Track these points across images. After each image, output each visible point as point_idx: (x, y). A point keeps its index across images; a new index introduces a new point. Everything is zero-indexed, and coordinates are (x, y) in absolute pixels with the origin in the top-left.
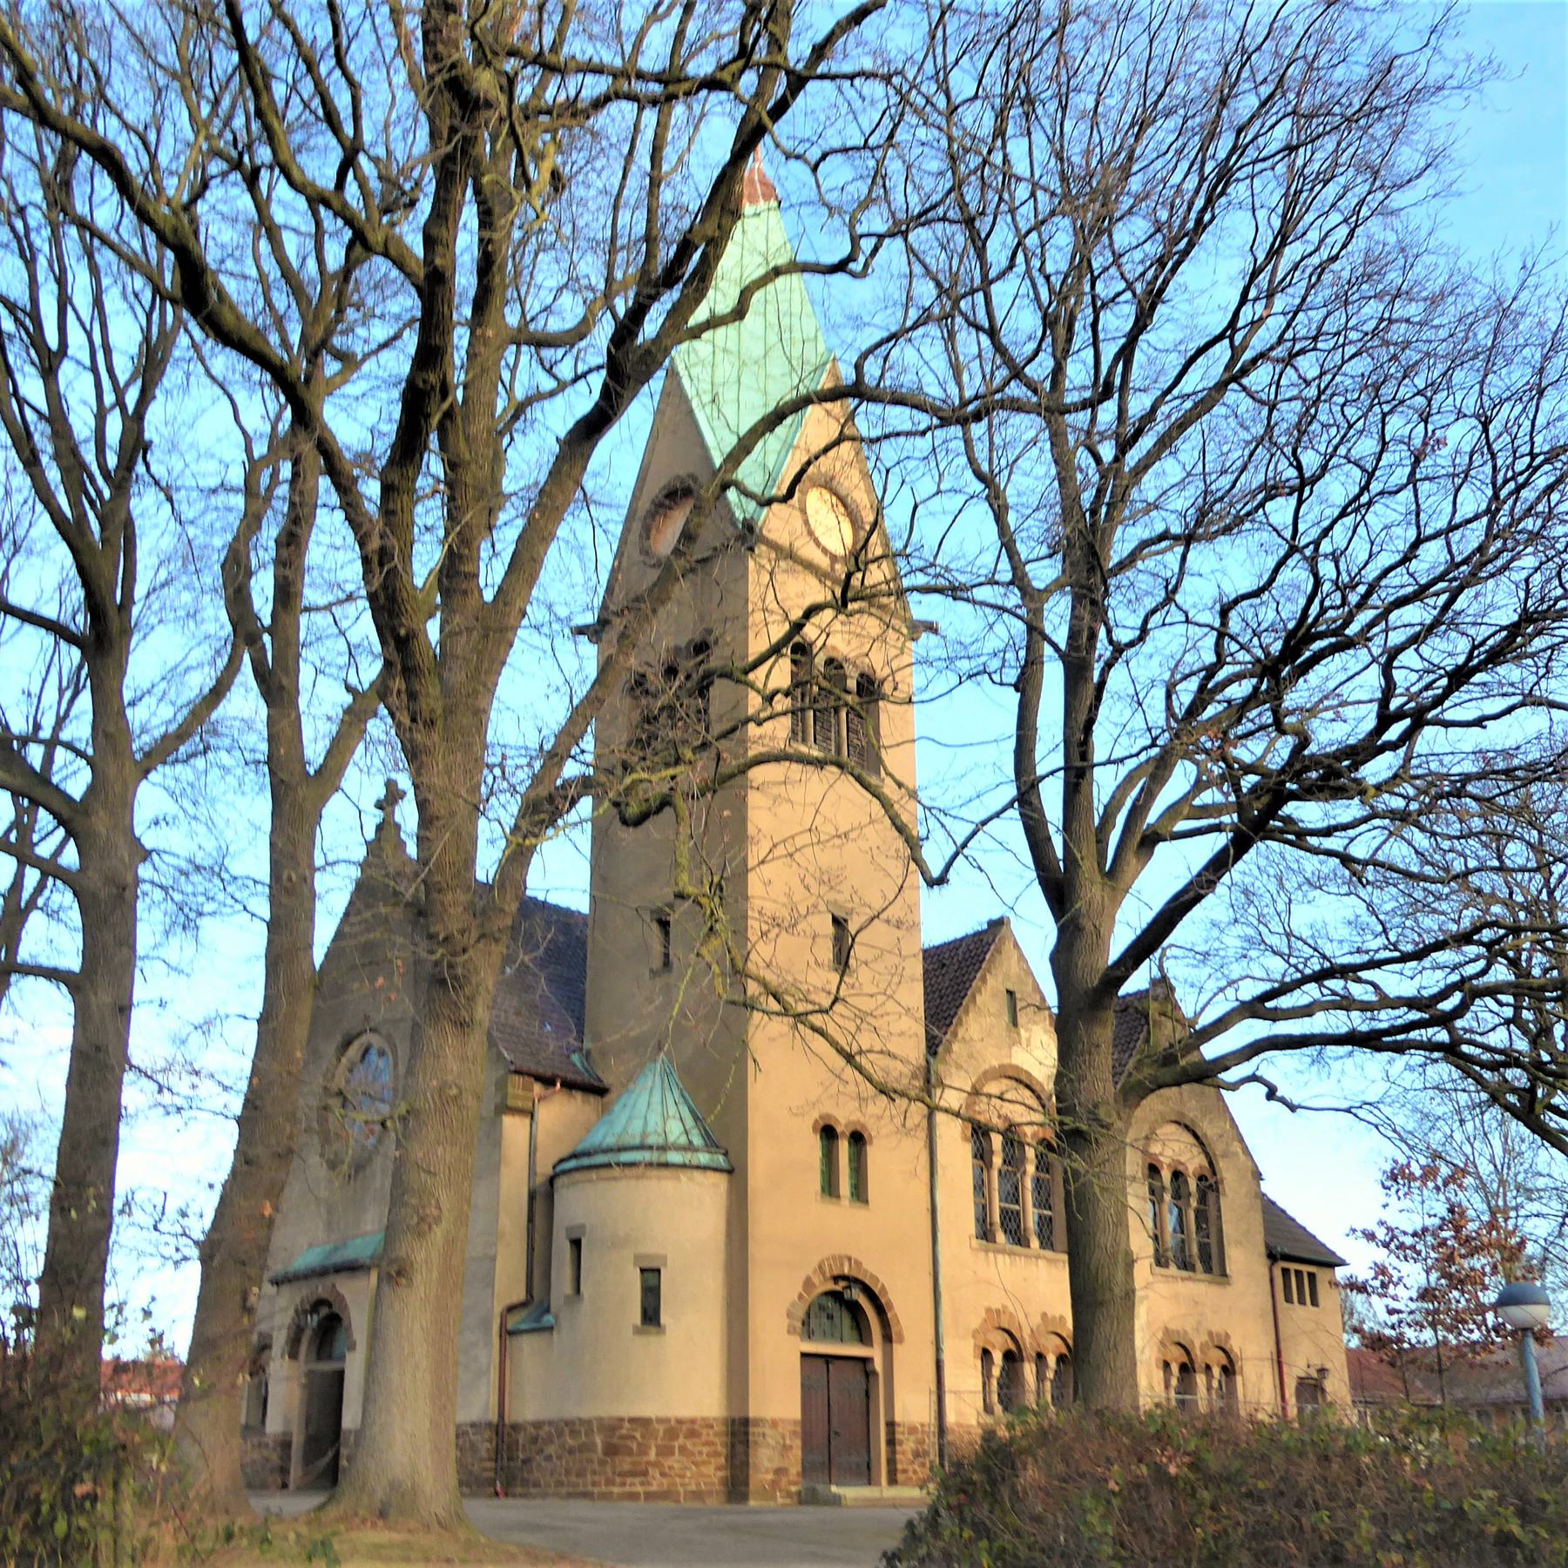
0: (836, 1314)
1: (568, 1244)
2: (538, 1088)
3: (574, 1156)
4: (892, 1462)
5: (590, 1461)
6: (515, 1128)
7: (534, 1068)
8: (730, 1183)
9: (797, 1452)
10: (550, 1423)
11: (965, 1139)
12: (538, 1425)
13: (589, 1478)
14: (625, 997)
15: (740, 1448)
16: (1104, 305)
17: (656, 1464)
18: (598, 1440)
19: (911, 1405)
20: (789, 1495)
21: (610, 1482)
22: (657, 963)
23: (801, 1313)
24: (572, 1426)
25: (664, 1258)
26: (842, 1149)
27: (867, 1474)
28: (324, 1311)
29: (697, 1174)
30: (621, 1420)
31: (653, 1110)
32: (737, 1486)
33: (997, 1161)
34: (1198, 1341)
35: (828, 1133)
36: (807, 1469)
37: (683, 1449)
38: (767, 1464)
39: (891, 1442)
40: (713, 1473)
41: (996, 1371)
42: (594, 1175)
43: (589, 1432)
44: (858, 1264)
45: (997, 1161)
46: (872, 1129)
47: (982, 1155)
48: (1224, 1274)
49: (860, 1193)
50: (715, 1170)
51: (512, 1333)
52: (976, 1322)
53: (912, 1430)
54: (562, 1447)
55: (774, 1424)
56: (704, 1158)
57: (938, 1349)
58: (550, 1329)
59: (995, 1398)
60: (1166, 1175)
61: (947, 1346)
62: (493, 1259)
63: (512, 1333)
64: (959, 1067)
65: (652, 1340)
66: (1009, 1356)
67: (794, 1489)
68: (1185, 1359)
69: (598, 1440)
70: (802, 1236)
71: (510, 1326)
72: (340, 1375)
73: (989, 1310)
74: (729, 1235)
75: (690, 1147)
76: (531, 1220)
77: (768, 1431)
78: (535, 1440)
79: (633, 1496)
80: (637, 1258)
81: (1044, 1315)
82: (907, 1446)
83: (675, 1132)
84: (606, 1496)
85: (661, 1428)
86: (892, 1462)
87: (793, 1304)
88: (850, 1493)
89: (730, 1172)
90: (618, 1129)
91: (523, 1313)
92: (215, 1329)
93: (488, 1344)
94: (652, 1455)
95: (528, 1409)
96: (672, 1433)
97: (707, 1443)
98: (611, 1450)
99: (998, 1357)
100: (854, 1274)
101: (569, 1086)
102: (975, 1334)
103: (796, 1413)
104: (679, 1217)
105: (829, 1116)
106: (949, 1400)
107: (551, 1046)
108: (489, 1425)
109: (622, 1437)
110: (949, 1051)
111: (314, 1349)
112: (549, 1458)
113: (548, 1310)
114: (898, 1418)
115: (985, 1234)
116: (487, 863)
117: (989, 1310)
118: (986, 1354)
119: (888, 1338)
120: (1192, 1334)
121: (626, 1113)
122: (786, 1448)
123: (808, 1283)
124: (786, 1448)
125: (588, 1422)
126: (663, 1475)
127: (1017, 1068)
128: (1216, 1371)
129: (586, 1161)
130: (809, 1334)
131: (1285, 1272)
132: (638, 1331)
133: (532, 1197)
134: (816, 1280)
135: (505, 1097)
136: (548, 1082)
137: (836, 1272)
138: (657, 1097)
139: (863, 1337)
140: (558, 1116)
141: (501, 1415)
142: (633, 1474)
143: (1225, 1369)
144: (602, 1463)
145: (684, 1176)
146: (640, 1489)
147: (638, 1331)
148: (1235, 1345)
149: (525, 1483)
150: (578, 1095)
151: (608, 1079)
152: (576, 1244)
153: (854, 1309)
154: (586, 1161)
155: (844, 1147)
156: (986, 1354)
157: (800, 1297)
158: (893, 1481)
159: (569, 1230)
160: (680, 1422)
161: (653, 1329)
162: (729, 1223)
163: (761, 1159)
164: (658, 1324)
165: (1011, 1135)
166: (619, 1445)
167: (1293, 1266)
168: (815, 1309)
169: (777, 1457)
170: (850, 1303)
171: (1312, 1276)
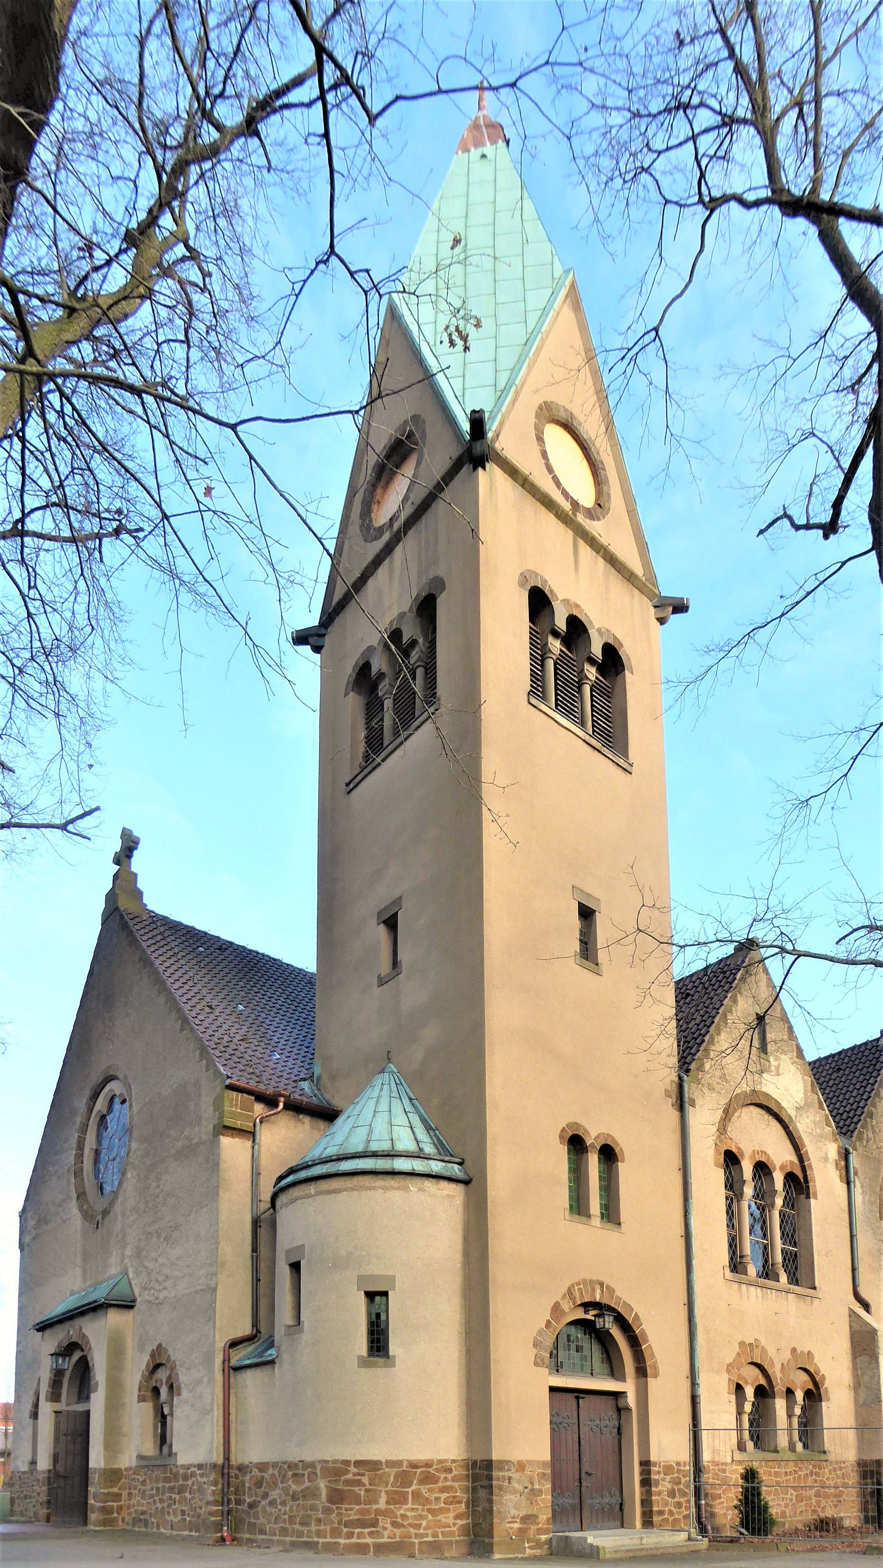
0: (586, 1344)
1: (287, 1270)
2: (259, 1109)
3: (292, 1171)
4: (646, 1503)
5: (313, 1508)
6: (233, 1149)
7: (253, 1085)
8: (467, 1195)
9: (547, 1497)
10: (275, 1465)
11: (717, 1165)
12: (262, 1467)
13: (313, 1528)
14: (354, 1018)
15: (482, 1493)
16: (578, 1398)
17: (386, 1513)
18: (322, 1485)
19: (668, 1444)
20: (539, 1544)
21: (336, 1533)
22: (385, 967)
23: (549, 1342)
24: (295, 1469)
25: (392, 1279)
26: (592, 1159)
27: (618, 1516)
28: (76, 1356)
29: (428, 1184)
30: (347, 1463)
31: (380, 1118)
32: (479, 1538)
33: (749, 1191)
35: (576, 1143)
36: (558, 1513)
37: (416, 1495)
38: (513, 1512)
39: (646, 1482)
40: (452, 1521)
41: (748, 1407)
42: (312, 1188)
43: (313, 1476)
44: (611, 1290)
45: (749, 1191)
46: (624, 1144)
47: (733, 1185)
49: (611, 1213)
50: (450, 1179)
51: (236, 1369)
53: (668, 1470)
54: (286, 1490)
55: (521, 1466)
56: (436, 1167)
57: (694, 1384)
58: (272, 1362)
59: (746, 1434)
61: (703, 1379)
62: (215, 1290)
63: (236, 1369)
64: (711, 1088)
65: (378, 1373)
67: (544, 1537)
68: (811, 1386)
69: (322, 1485)
70: (548, 1254)
71: (234, 1362)
72: (87, 1413)
73: (742, 1344)
74: (466, 1254)
75: (419, 1155)
76: (255, 1249)
77: (515, 1476)
78: (259, 1484)
79: (362, 1549)
80: (361, 1279)
81: (794, 1350)
82: (663, 1485)
83: (405, 1143)
84: (331, 1548)
85: (393, 1471)
87: (540, 1333)
88: (605, 1539)
89: (466, 1182)
90: (339, 1139)
91: (251, 1348)
92: (557, 1420)
93: (211, 1380)
94: (382, 1504)
95: (252, 1451)
96: (404, 1478)
97: (444, 1490)
98: (337, 1497)
99: (750, 1392)
100: (605, 1301)
101: (296, 1108)
102: (729, 1368)
103: (545, 1455)
104: (409, 1232)
105: (577, 1125)
106: (705, 1436)
107: (277, 1069)
108: (214, 1466)
109: (348, 1482)
110: (700, 1068)
111: (75, 1391)
112: (272, 1503)
113: (271, 1345)
117: (742, 1344)
118: (739, 1388)
119: (642, 1372)
121: (350, 1122)
122: (535, 1493)
123: (556, 1308)
124: (535, 1493)
125: (312, 1465)
126: (395, 1524)
127: (767, 1095)
129: (303, 1175)
130: (558, 1368)
132: (363, 1363)
133: (256, 1223)
134: (566, 1306)
135: (221, 1117)
136: (270, 1101)
137: (587, 1299)
138: (383, 1106)
139: (614, 1370)
140: (283, 1139)
141: (227, 1458)
142: (362, 1524)
143: (808, 1394)
144: (327, 1511)
145: (413, 1185)
146: (369, 1540)
147: (363, 1363)
149: (252, 1527)
150: (307, 1120)
151: (337, 1103)
152: (296, 1267)
153: (604, 1340)
154: (303, 1175)
155: (593, 1161)
156: (739, 1388)
159: (288, 1252)
160: (414, 1465)
161: (381, 1360)
162: (466, 1239)
163: (501, 1169)
164: (387, 1355)
165: (762, 1169)
166: (347, 1487)
168: (563, 1340)
169: (524, 1505)
170: (600, 1330)
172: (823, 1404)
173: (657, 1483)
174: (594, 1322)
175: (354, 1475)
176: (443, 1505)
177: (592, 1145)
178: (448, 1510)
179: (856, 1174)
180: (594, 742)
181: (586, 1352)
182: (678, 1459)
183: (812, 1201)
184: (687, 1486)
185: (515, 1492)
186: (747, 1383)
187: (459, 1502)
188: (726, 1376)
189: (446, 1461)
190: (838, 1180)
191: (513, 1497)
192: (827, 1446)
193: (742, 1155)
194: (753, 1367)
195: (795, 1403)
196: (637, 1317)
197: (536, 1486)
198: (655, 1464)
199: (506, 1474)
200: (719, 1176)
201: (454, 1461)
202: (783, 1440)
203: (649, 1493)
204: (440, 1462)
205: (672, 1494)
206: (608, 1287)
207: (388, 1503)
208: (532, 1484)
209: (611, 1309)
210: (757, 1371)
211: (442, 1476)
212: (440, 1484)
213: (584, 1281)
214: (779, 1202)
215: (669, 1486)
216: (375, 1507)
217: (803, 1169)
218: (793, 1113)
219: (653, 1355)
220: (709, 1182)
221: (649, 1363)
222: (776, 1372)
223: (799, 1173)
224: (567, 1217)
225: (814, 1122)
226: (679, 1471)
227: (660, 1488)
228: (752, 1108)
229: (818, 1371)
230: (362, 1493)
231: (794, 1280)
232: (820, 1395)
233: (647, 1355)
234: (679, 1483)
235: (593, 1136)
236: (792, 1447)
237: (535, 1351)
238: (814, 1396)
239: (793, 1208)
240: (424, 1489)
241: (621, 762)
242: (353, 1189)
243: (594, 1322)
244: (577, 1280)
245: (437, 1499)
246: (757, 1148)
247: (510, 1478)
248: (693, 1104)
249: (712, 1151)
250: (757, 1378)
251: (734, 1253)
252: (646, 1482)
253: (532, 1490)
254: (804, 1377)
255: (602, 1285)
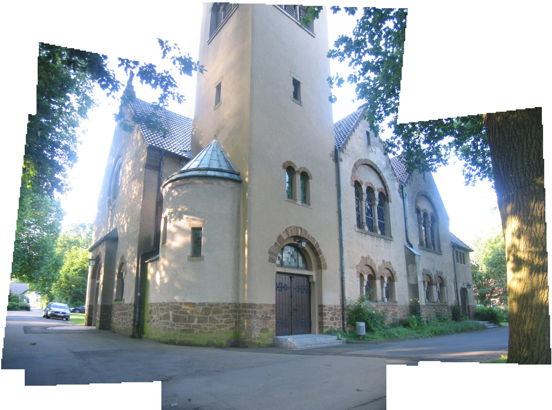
11: (352, 185)
16: (291, 277)
18: (171, 313)
19: (330, 298)
29: (222, 182)
33: (365, 197)
34: (433, 274)
35: (290, 169)
37: (212, 319)
44: (306, 232)
45: (365, 197)
46: (312, 171)
47: (358, 194)
48: (440, 250)
49: (305, 199)
52: (358, 262)
53: (330, 309)
55: (261, 306)
60: (422, 213)
66: (370, 277)
68: (390, 276)
73: (362, 257)
77: (258, 311)
81: (383, 261)
86: (321, 323)
87: (272, 247)
94: (196, 323)
97: (225, 316)
99: (366, 277)
100: (303, 236)
102: (357, 267)
114: (324, 303)
115: (360, 225)
116: (395, 49)
117: (362, 257)
118: (361, 275)
120: (432, 272)
124: (267, 318)
128: (386, 279)
131: (457, 252)
143: (389, 278)
148: (444, 276)
155: (298, 177)
156: (361, 275)
157: (276, 244)
158: (321, 332)
160: (211, 305)
165: (370, 190)
167: (459, 250)
170: (304, 247)
171: (463, 254)
172: (395, 283)
173: (325, 314)
174: (298, 245)
175: (188, 309)
176: (224, 323)
177: (298, 171)
178: (226, 326)
179: (406, 195)
180: (299, 23)
181: (296, 257)
182: (335, 304)
183: (390, 204)
184: (339, 316)
185: (257, 318)
186: (364, 273)
187: (232, 322)
188: (356, 270)
189: (226, 303)
190: (399, 197)
191: (256, 320)
192: (397, 299)
193: (362, 183)
194: (367, 267)
195: (384, 282)
196: (317, 243)
197: (268, 315)
198: (325, 306)
199: (253, 310)
200: (353, 189)
201: (229, 304)
202: (379, 298)
203: (322, 319)
204: (224, 304)
205: (332, 319)
206: (304, 230)
207: (198, 322)
208: (266, 314)
209: (304, 239)
210: (369, 269)
211: (224, 310)
212: (223, 314)
213: (293, 227)
214: (377, 203)
215: (331, 316)
216: (192, 324)
217: (386, 191)
218: (382, 170)
219: (324, 260)
220: (349, 192)
221: (322, 263)
222: (377, 269)
223: (384, 192)
224: (286, 199)
225: (390, 175)
226: (335, 309)
227: (327, 316)
228: (366, 166)
229: (393, 270)
230: (187, 317)
231: (383, 233)
232: (394, 279)
233: (322, 260)
234: (335, 314)
235: (299, 165)
236: (383, 300)
237: (269, 255)
238: (392, 279)
239: (382, 206)
240: (215, 316)
241: (311, 33)
242: (189, 184)
243: (298, 245)
244: (290, 226)
245: (221, 321)
246: (368, 181)
247: (255, 312)
248: (341, 160)
249: (350, 180)
250: (369, 272)
251: (360, 221)
252: (321, 314)
253: (266, 317)
254: (388, 272)
255: (301, 229)
